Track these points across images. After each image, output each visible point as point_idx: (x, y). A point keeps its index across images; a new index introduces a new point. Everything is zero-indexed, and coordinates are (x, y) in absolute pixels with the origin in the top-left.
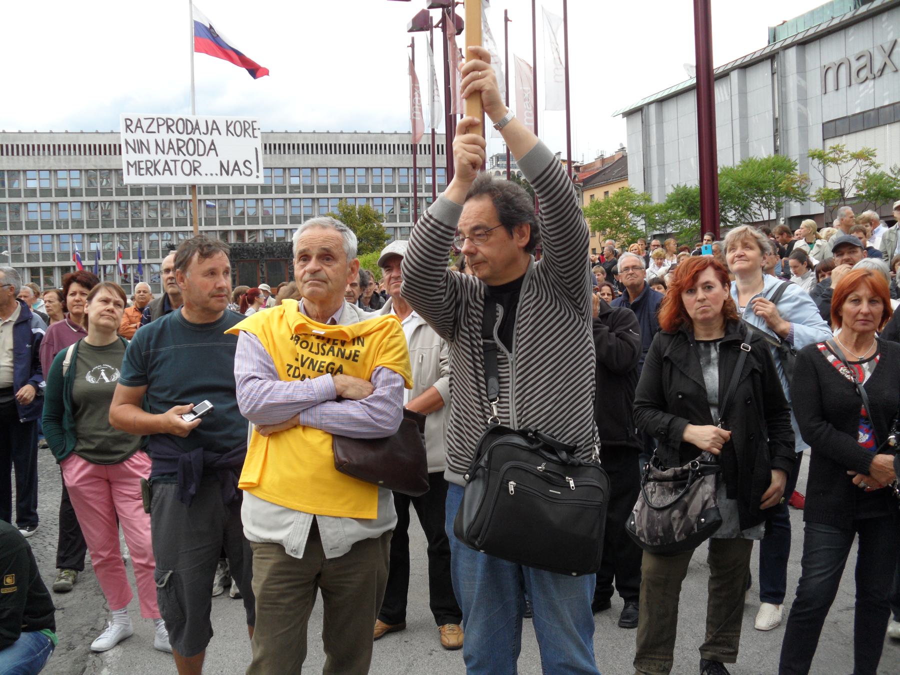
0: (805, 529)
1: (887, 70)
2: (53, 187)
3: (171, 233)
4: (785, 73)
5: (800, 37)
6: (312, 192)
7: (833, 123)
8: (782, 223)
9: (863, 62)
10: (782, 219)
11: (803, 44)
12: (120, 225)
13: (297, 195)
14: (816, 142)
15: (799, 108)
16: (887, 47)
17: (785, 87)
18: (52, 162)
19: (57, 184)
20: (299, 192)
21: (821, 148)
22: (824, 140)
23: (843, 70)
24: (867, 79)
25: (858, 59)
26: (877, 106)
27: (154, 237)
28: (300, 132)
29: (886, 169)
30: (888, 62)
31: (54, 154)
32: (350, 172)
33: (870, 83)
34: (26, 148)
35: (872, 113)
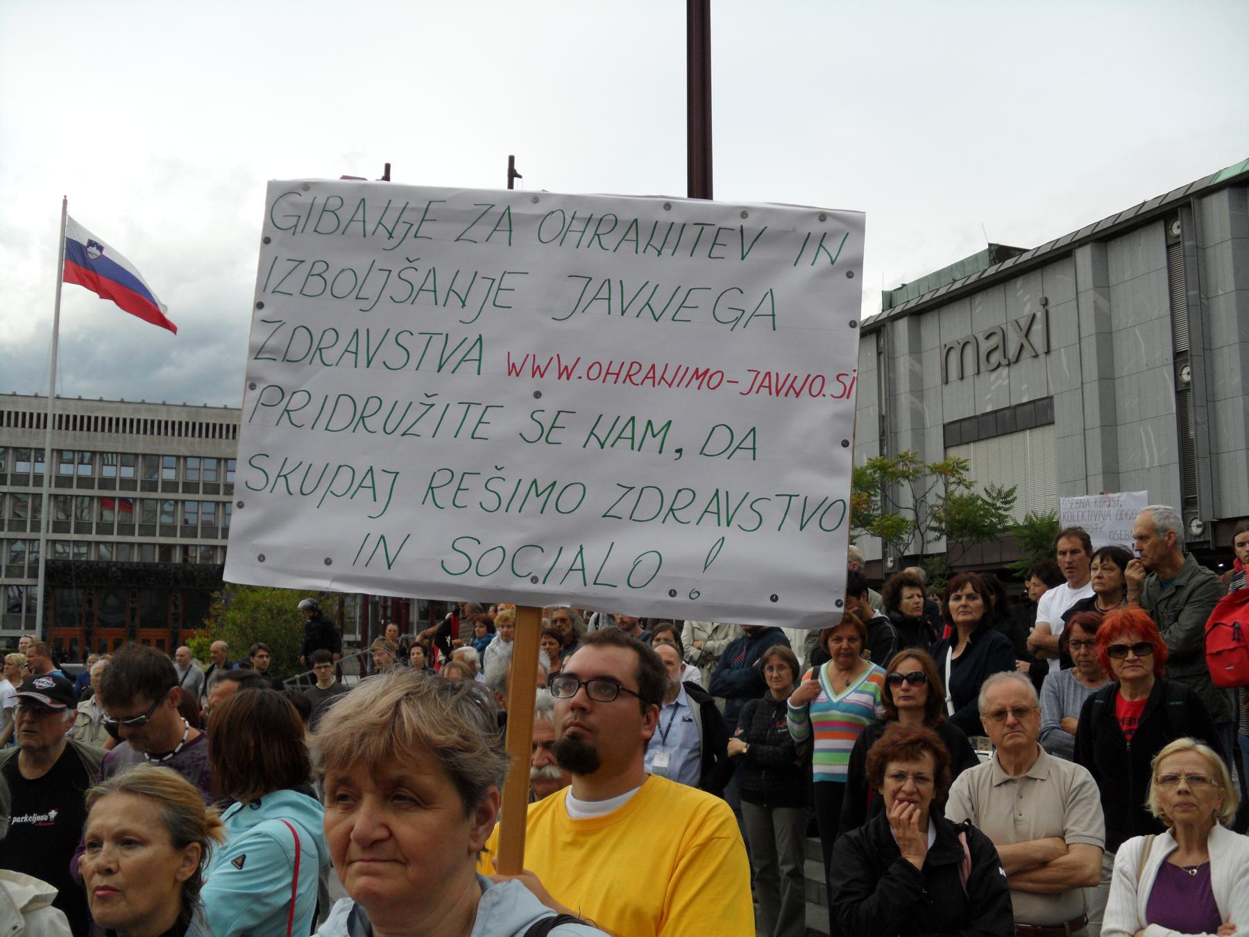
0: (1208, 933)
1: (1025, 354)
2: (97, 476)
3: (89, 543)
4: (893, 353)
5: (912, 304)
7: (958, 425)
8: (890, 564)
9: (994, 341)
10: (890, 559)
11: (918, 313)
12: (121, 532)
14: (934, 452)
15: (912, 403)
16: (1024, 323)
17: (894, 372)
19: (185, 476)
21: (942, 461)
22: (945, 448)
23: (969, 351)
24: (999, 365)
25: (988, 338)
26: (1014, 403)
27: (18, 546)
28: (143, 402)
29: (978, 490)
30: (1026, 344)
31: (180, 435)
33: (1004, 371)
34: (177, 427)
35: (1008, 413)
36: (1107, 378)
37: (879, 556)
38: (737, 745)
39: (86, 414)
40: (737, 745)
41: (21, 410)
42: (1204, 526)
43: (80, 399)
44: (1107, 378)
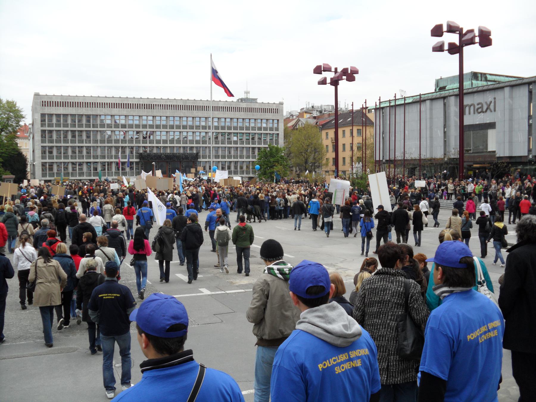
6: (206, 129)
9: (480, 106)
13: (199, 131)
16: (488, 103)
23: (472, 108)
32: (185, 119)
33: (482, 114)
34: (297, 229)
36: (511, 120)
37: (443, 157)
38: (477, 171)
39: (150, 104)
40: (477, 171)
41: (129, 103)
42: (533, 156)
43: (120, 97)
44: (511, 120)
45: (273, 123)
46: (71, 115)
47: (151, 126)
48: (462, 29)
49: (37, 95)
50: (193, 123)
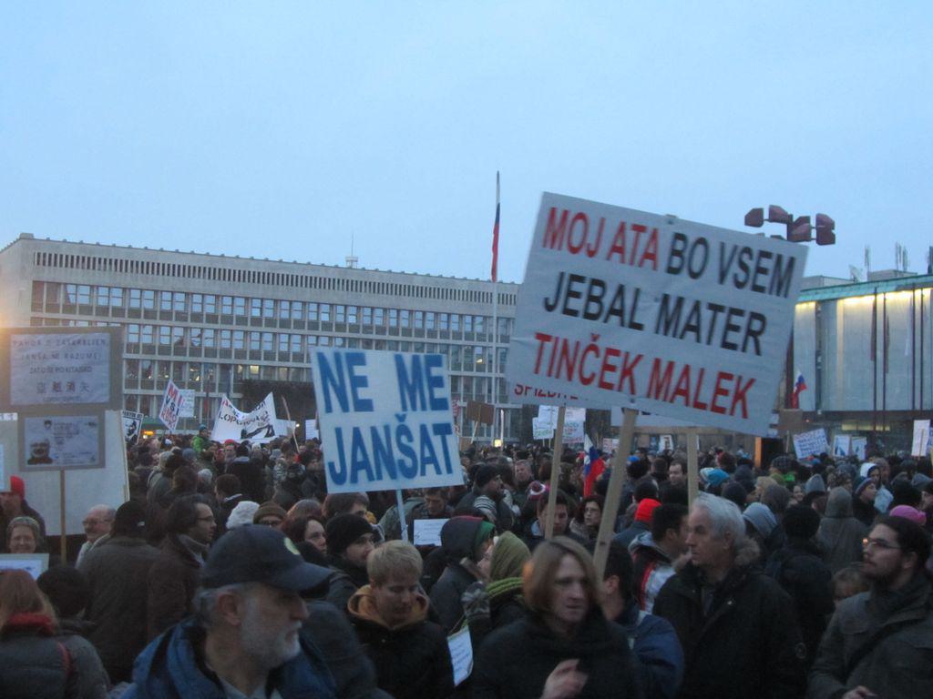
13: (259, 329)
18: (309, 294)
20: (372, 333)
41: (228, 268)
45: (372, 316)
46: (48, 282)
47: (118, 312)
48: (791, 216)
49: (26, 238)
50: (275, 313)
